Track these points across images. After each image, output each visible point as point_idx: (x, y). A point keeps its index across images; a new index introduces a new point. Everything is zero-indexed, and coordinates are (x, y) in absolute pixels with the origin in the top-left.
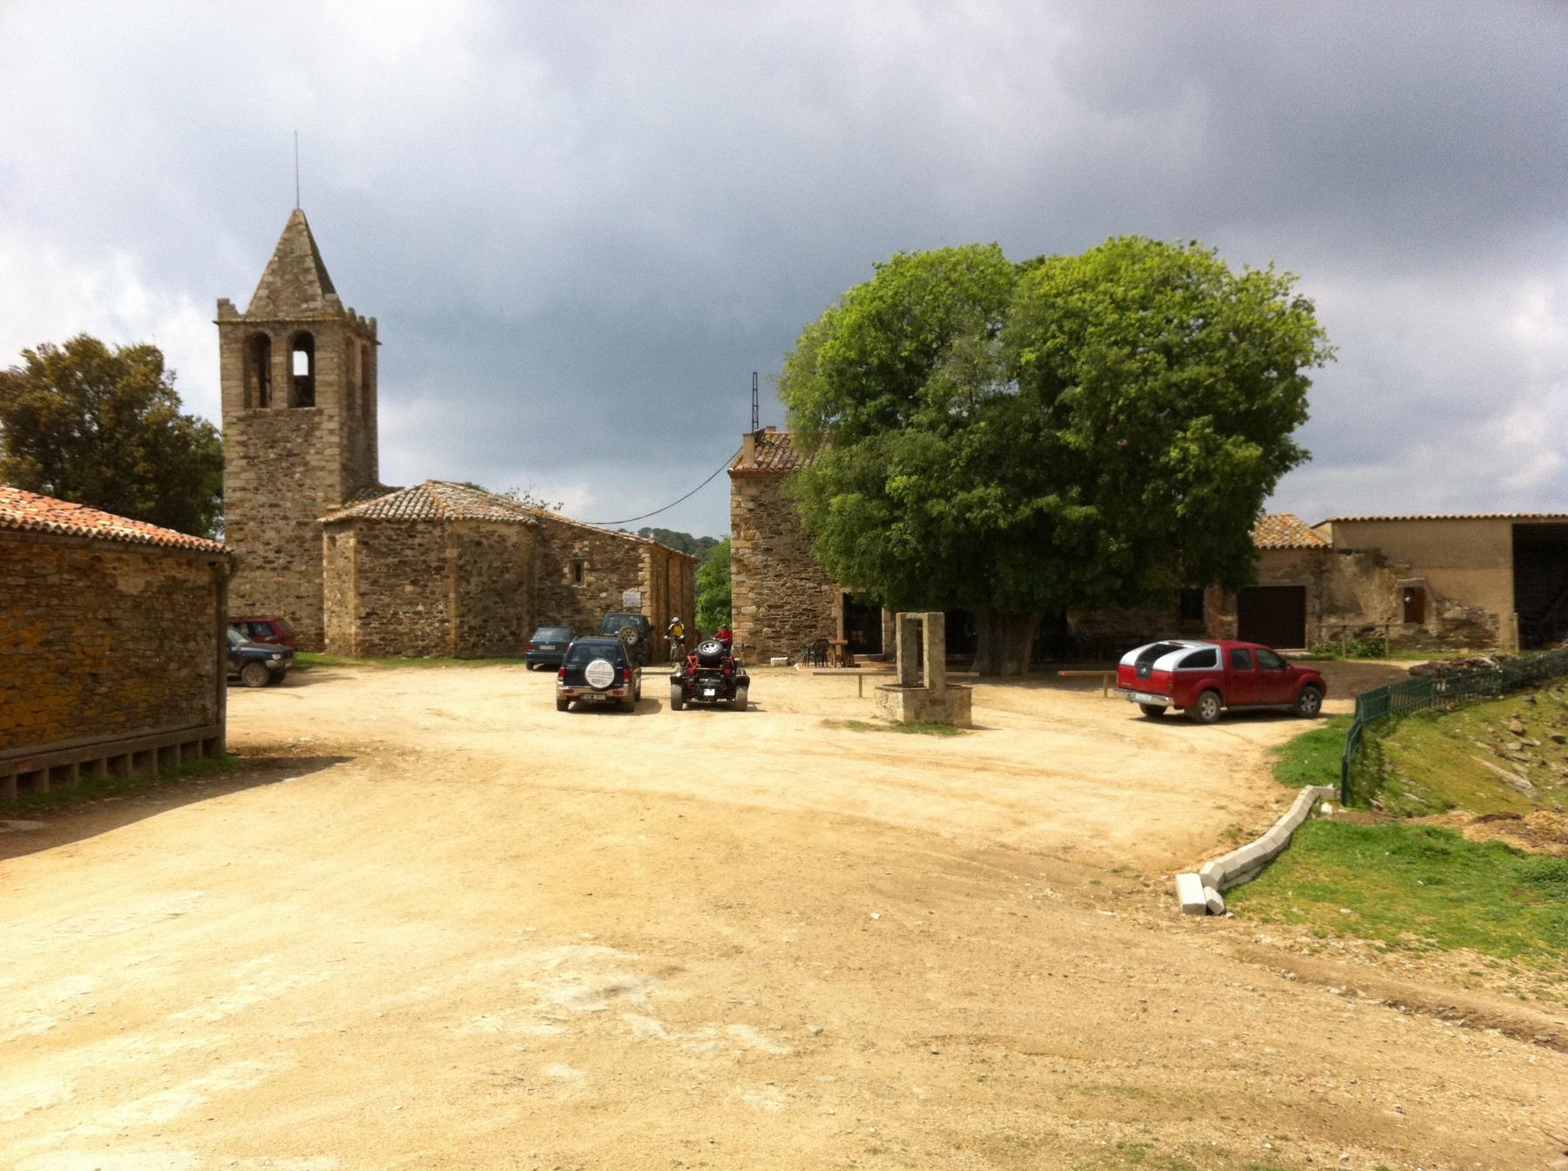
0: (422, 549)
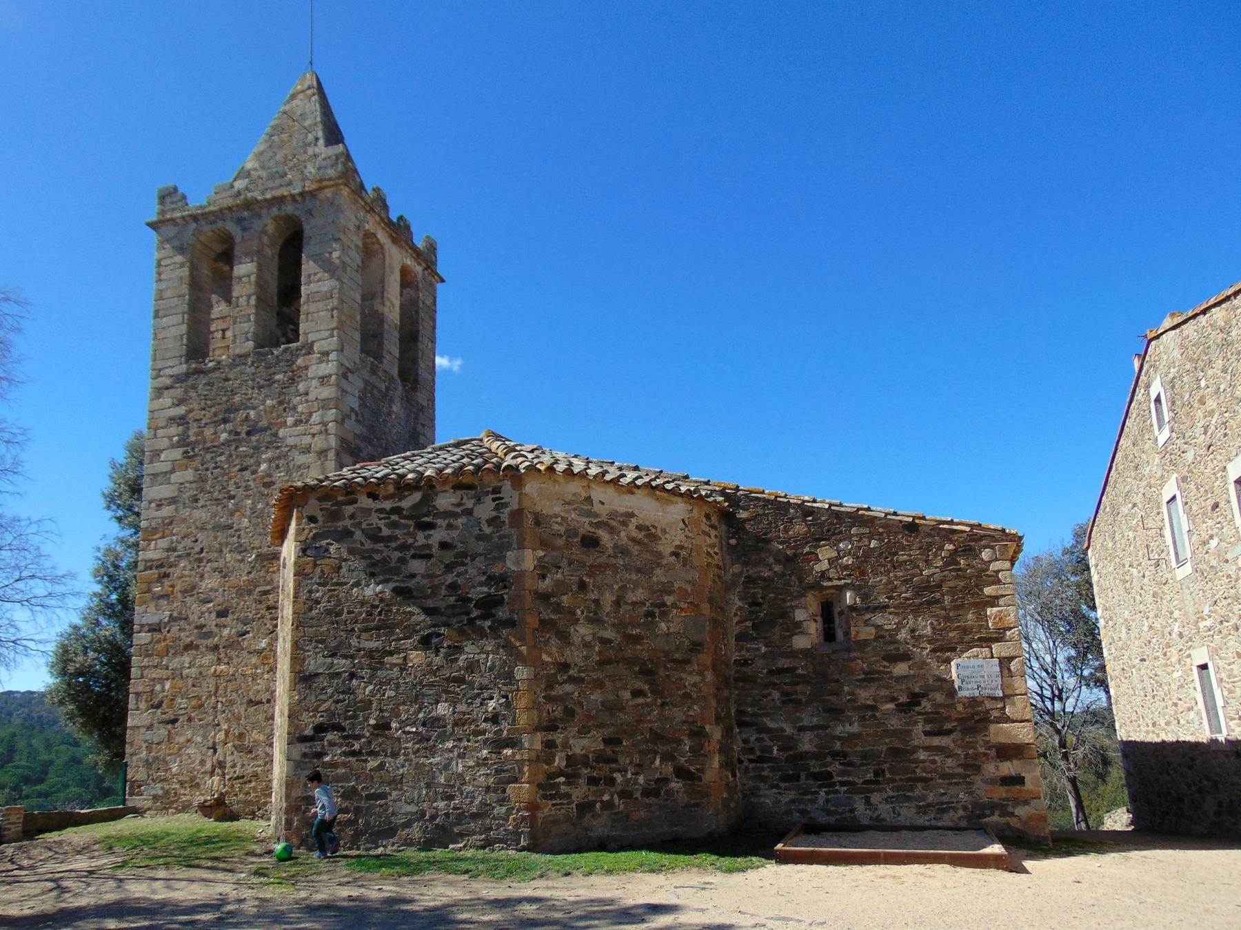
0: (449, 557)
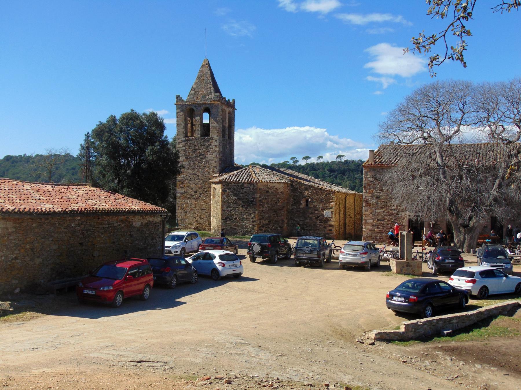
0: (246, 194)
